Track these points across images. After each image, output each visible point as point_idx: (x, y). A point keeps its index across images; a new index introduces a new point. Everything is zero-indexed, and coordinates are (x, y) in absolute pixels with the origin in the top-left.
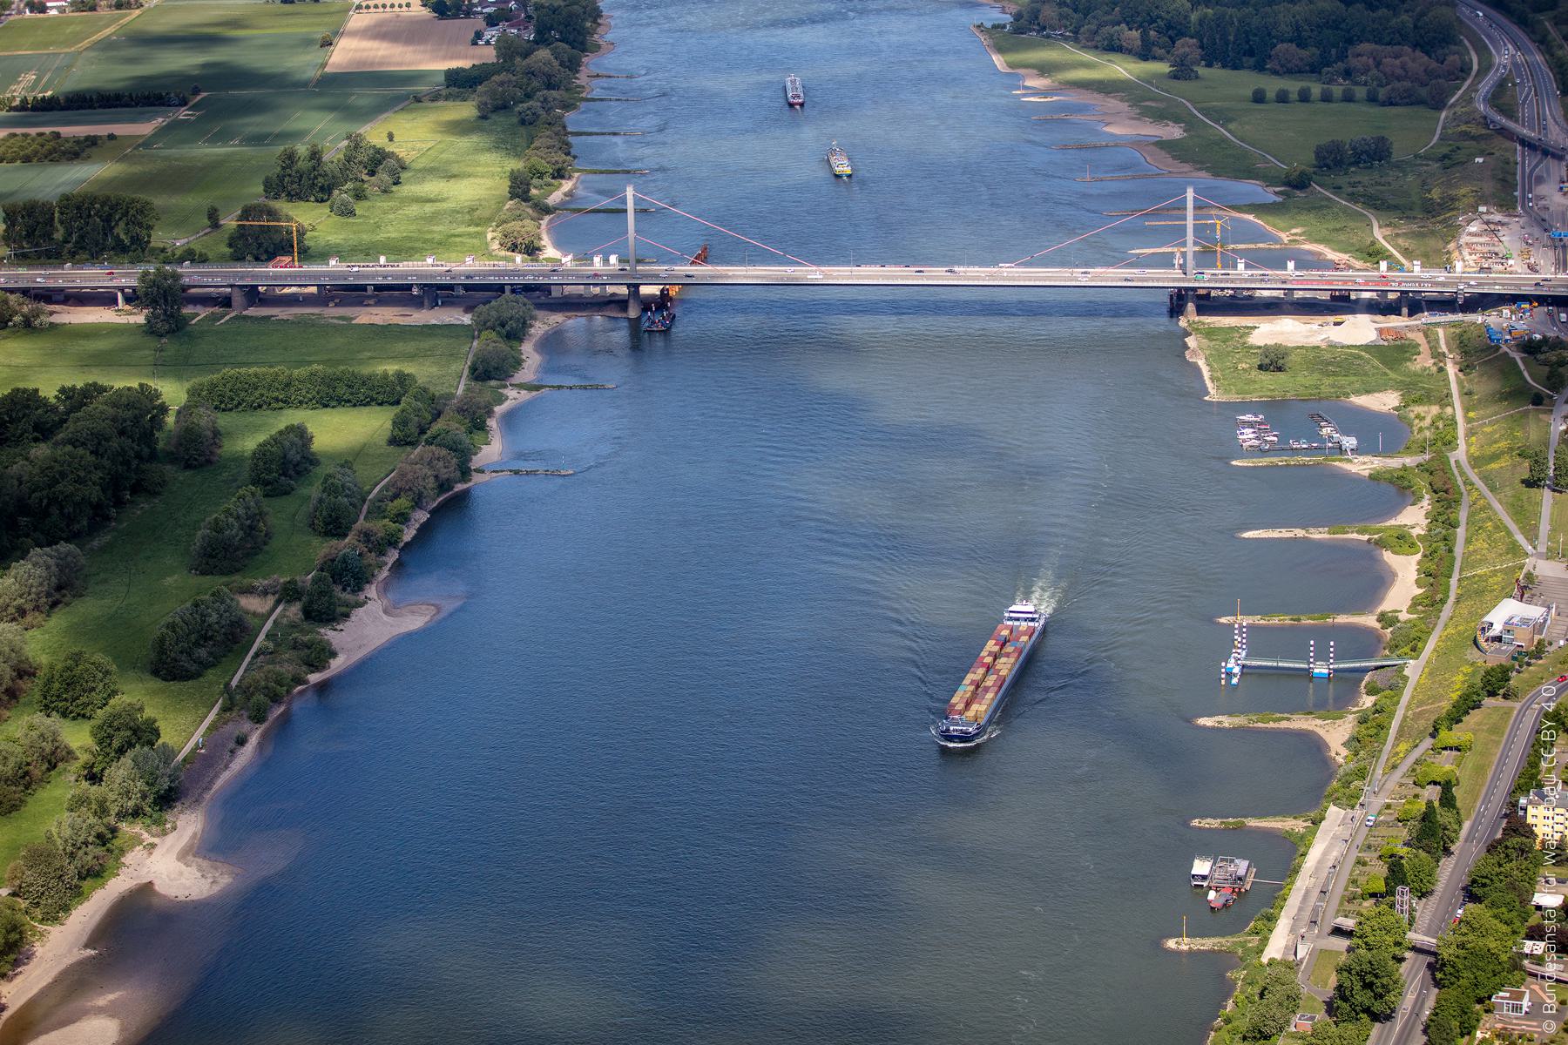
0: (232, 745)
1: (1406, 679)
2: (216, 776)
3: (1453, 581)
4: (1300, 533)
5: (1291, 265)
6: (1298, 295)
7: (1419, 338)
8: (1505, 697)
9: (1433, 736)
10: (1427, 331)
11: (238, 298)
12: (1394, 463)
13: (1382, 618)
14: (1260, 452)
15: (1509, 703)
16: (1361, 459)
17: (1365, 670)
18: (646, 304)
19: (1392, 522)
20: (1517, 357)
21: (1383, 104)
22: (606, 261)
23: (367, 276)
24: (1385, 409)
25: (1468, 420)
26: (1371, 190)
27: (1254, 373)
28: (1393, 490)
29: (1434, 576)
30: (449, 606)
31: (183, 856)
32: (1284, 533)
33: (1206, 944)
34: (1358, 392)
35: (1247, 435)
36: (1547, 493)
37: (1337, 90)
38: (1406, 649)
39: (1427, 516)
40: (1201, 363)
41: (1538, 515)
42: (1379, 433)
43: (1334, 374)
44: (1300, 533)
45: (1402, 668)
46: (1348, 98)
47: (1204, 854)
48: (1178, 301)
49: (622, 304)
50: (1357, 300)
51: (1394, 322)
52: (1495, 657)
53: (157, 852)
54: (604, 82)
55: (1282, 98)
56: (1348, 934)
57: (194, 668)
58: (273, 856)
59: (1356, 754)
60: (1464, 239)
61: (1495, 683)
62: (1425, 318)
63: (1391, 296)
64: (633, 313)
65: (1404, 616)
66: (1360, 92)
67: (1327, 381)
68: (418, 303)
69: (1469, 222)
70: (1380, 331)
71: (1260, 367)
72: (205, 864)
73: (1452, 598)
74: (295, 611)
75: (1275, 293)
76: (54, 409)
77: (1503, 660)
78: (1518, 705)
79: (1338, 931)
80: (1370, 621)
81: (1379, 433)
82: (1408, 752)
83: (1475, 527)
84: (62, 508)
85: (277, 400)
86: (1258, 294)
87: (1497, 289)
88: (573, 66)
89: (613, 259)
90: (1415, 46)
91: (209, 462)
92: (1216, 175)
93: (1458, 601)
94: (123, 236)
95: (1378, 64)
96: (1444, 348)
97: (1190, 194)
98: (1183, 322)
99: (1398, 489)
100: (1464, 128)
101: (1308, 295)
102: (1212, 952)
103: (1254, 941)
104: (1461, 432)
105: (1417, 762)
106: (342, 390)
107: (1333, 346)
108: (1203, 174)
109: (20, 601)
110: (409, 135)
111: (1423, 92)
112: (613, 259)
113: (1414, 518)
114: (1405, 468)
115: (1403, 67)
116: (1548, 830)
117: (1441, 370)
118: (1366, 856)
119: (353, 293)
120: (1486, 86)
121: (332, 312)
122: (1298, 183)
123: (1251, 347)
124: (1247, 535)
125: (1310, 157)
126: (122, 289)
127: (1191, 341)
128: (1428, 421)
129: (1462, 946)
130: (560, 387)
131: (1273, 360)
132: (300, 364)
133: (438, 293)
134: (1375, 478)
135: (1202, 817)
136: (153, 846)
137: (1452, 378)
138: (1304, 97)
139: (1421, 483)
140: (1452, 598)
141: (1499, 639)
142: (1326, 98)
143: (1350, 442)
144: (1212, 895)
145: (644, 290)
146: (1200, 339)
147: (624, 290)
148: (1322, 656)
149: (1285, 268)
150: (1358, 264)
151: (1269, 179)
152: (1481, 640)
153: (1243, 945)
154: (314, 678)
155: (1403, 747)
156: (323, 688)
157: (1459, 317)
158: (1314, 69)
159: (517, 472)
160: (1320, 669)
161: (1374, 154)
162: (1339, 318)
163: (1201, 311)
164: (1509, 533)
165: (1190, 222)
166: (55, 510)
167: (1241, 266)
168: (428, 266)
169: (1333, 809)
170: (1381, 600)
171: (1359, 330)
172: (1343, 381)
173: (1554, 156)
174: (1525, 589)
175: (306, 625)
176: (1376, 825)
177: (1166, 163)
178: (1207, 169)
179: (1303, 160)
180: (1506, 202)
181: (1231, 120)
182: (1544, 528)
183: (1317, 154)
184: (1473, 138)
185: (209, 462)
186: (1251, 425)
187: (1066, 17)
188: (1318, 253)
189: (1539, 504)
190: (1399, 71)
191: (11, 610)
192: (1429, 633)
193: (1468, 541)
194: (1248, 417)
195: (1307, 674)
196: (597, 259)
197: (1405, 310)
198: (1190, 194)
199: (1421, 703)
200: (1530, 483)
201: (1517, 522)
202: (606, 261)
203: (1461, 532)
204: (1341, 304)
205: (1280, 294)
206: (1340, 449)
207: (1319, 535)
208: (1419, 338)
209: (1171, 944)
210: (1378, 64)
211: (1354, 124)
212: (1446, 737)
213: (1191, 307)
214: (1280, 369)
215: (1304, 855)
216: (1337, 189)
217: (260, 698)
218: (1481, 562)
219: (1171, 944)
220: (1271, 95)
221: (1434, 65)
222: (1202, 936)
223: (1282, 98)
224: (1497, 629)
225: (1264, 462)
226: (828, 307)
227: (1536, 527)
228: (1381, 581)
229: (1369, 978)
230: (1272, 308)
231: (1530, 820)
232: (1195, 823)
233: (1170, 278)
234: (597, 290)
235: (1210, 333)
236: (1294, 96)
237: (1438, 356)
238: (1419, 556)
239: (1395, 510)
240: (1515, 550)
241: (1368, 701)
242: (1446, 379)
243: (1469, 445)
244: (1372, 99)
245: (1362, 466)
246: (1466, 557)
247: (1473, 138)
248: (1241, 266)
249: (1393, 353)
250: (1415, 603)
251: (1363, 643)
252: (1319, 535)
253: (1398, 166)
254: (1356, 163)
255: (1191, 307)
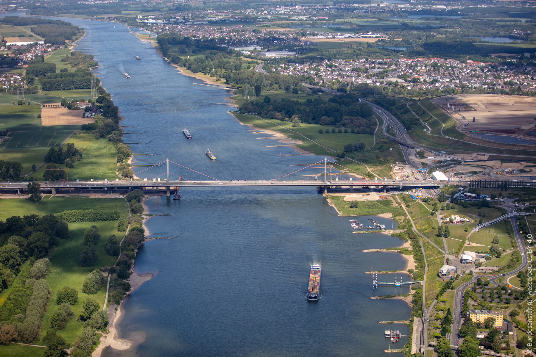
0: (114, 311)
1: (422, 286)
2: (114, 319)
3: (425, 261)
4: (379, 250)
5: (351, 179)
6: (354, 187)
7: (391, 198)
8: (451, 289)
9: (437, 299)
10: (393, 196)
11: (54, 191)
12: (398, 232)
13: (409, 271)
14: (359, 229)
15: (453, 291)
16: (387, 231)
17: (410, 284)
18: (172, 192)
19: (402, 247)
20: (422, 203)
21: (356, 133)
22: (157, 180)
23: (89, 185)
24: (389, 218)
25: (413, 220)
26: (363, 158)
27: (350, 209)
28: (398, 238)
29: (419, 259)
30: (156, 274)
31: (115, 339)
32: (375, 251)
33: (396, 351)
34: (380, 213)
35: (354, 225)
36: (444, 239)
37: (343, 130)
38: (420, 278)
39: (411, 245)
40: (334, 206)
41: (443, 244)
42: (389, 224)
43: (372, 208)
44: (379, 250)
45: (420, 283)
46: (346, 132)
47: (388, 329)
48: (321, 190)
49: (165, 192)
50: (370, 189)
51: (384, 194)
52: (447, 279)
53: (107, 338)
54: (128, 129)
55: (327, 132)
56: (433, 346)
57: (95, 291)
58: (140, 337)
59: (416, 304)
60: (395, 171)
61: (448, 286)
62: (391, 193)
63: (380, 187)
64: (168, 194)
65: (415, 270)
66: (349, 130)
67: (371, 210)
68: (106, 192)
69: (394, 167)
70: (380, 197)
71: (351, 207)
72: (122, 341)
73: (426, 266)
74: (115, 275)
75: (347, 187)
76: (23, 222)
77: (448, 280)
78: (455, 291)
79: (430, 346)
80: (406, 272)
81: (389, 224)
82: (431, 303)
83: (426, 249)
84: (38, 249)
85: (80, 219)
86: (342, 187)
87: (411, 185)
88: (117, 123)
89: (159, 179)
90: (363, 117)
91: (69, 237)
92: (316, 154)
93: (428, 266)
94: (12, 174)
95: (352, 122)
96: (399, 201)
97: (167, 160)
98: (324, 195)
99: (401, 238)
100: (382, 140)
101: (356, 187)
102: (397, 352)
103: (407, 350)
104: (412, 222)
105: (435, 305)
106: (98, 216)
107: (368, 201)
108: (312, 154)
109: (38, 274)
110: (80, 144)
111: (368, 130)
112: (159, 179)
113: (408, 245)
114: (401, 233)
115: (360, 122)
116: (475, 320)
117: (401, 207)
118: (430, 328)
119: (85, 190)
120: (384, 127)
121: (82, 195)
122: (341, 156)
123: (346, 202)
124: (364, 251)
125: (343, 149)
126: (19, 189)
127: (328, 200)
128: (402, 221)
129: (466, 347)
130: (157, 215)
131: (354, 205)
132: (86, 209)
133: (111, 189)
134: (393, 235)
135: (382, 321)
136: (106, 336)
137: (405, 209)
138: (333, 132)
139: (406, 237)
140: (426, 266)
141: (445, 275)
142: (340, 132)
143: (383, 226)
144: (392, 339)
145: (171, 188)
146: (330, 198)
147: (163, 188)
148: (399, 281)
149: (349, 180)
150: (367, 179)
151: (332, 155)
152: (440, 275)
153: (405, 350)
154: (128, 293)
155: (429, 302)
156: (129, 296)
157: (401, 192)
158: (333, 123)
159: (156, 238)
160: (398, 284)
161: (361, 148)
162: (368, 193)
163: (328, 192)
164: (437, 249)
165: (325, 167)
166: (36, 250)
167: (337, 179)
168: (106, 182)
169: (415, 318)
170: (407, 267)
171: (374, 197)
172: (375, 210)
173: (411, 148)
174: (448, 262)
175: (119, 279)
176: (430, 321)
177: (301, 151)
178: (313, 153)
179: (340, 150)
180: (403, 161)
181: (315, 138)
182: (446, 247)
183: (345, 148)
184: (386, 143)
185: (69, 237)
186: (354, 222)
187: (256, 109)
188: (355, 176)
189: (442, 241)
190: (359, 124)
191: (36, 277)
192: (424, 274)
193: (425, 251)
194: (353, 220)
195: (395, 286)
196: (154, 180)
197: (385, 191)
198: (167, 160)
199: (429, 292)
200: (439, 236)
201: (438, 246)
202: (157, 180)
203: (422, 248)
204: (366, 189)
205: (348, 187)
206: (380, 228)
207: (384, 251)
208: (391, 198)
209: (386, 351)
210: (352, 122)
211: (352, 139)
212: (441, 299)
213: (326, 191)
214: (356, 207)
215: (412, 329)
216: (353, 158)
217: (117, 298)
218: (432, 256)
219: (386, 351)
220: (324, 131)
221: (368, 122)
222: (394, 349)
223: (327, 132)
224: (444, 272)
225: (361, 232)
226: (254, 192)
227: (444, 247)
228: (404, 263)
229: (447, 354)
230: (347, 191)
231: (471, 317)
232: (380, 322)
233: (319, 183)
234: (155, 188)
235: (333, 198)
236: (331, 131)
237: (399, 204)
238: (413, 255)
239: (402, 244)
240: (439, 252)
241: (414, 292)
242: (403, 209)
243: (416, 227)
244: (353, 132)
245: (388, 232)
246: (426, 255)
247: (386, 143)
248: (337, 179)
249: (386, 203)
250: (417, 267)
251: (407, 277)
252: (384, 251)
253: (367, 151)
254: (356, 150)
255: (326, 191)
